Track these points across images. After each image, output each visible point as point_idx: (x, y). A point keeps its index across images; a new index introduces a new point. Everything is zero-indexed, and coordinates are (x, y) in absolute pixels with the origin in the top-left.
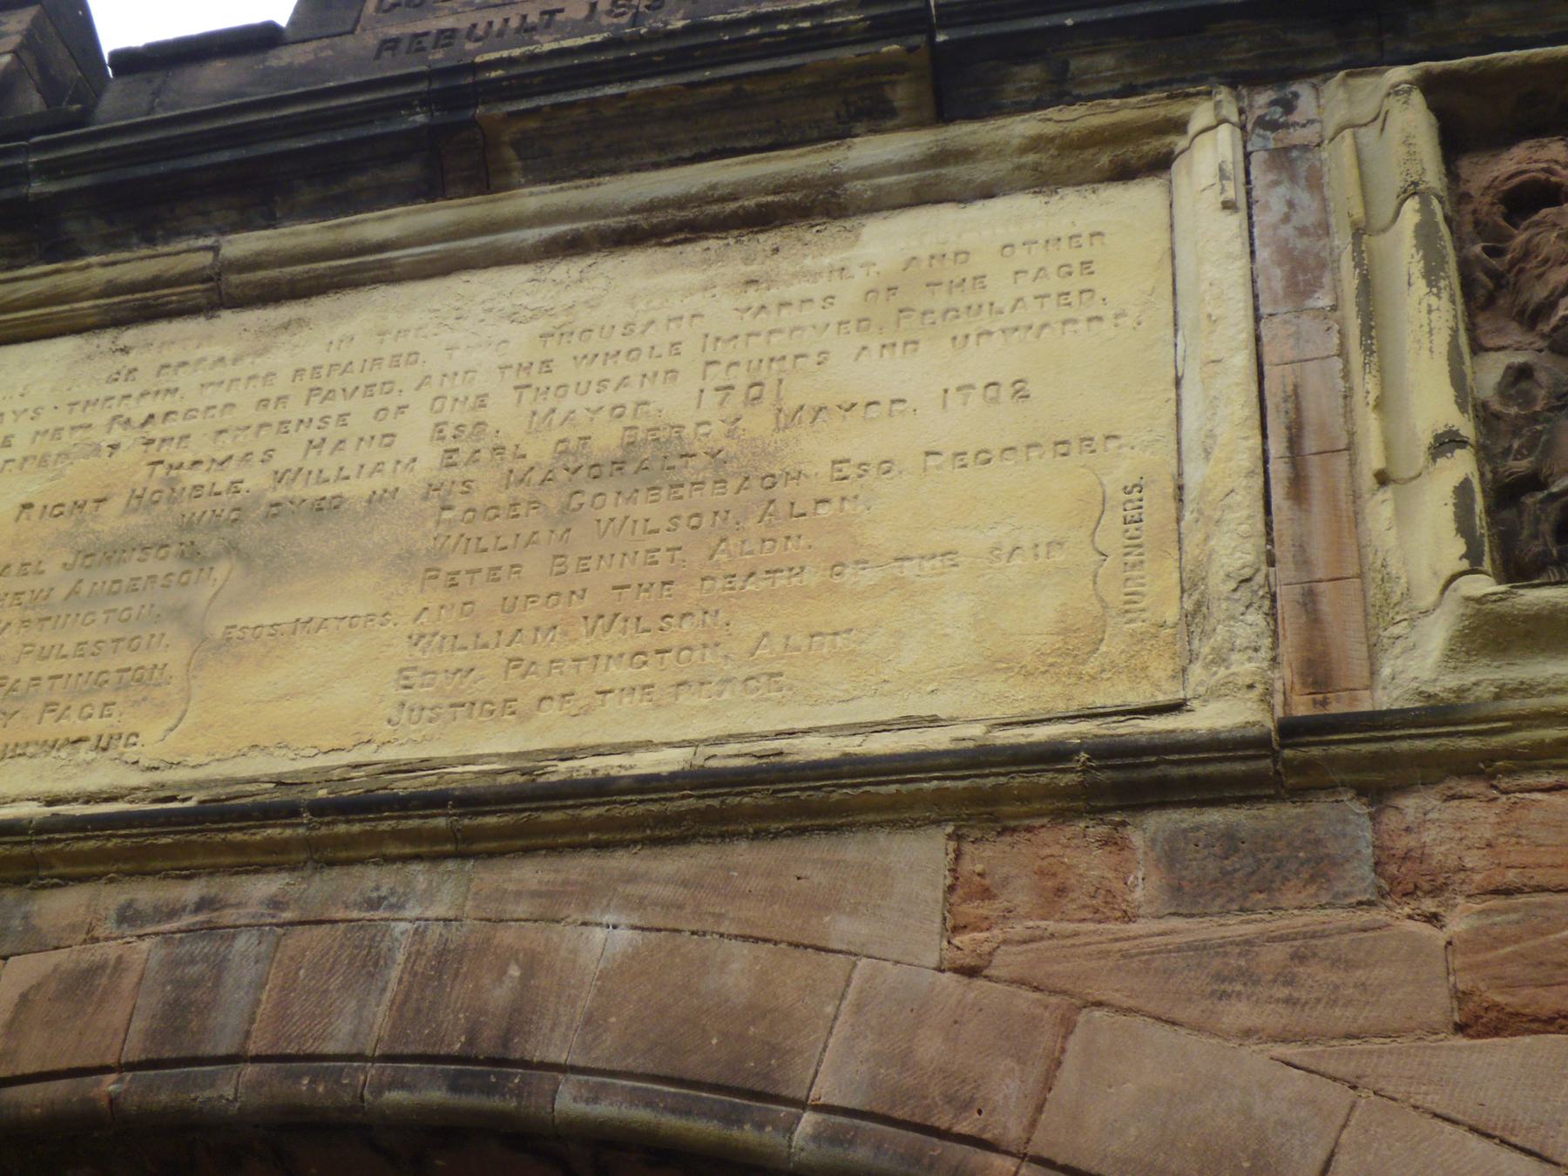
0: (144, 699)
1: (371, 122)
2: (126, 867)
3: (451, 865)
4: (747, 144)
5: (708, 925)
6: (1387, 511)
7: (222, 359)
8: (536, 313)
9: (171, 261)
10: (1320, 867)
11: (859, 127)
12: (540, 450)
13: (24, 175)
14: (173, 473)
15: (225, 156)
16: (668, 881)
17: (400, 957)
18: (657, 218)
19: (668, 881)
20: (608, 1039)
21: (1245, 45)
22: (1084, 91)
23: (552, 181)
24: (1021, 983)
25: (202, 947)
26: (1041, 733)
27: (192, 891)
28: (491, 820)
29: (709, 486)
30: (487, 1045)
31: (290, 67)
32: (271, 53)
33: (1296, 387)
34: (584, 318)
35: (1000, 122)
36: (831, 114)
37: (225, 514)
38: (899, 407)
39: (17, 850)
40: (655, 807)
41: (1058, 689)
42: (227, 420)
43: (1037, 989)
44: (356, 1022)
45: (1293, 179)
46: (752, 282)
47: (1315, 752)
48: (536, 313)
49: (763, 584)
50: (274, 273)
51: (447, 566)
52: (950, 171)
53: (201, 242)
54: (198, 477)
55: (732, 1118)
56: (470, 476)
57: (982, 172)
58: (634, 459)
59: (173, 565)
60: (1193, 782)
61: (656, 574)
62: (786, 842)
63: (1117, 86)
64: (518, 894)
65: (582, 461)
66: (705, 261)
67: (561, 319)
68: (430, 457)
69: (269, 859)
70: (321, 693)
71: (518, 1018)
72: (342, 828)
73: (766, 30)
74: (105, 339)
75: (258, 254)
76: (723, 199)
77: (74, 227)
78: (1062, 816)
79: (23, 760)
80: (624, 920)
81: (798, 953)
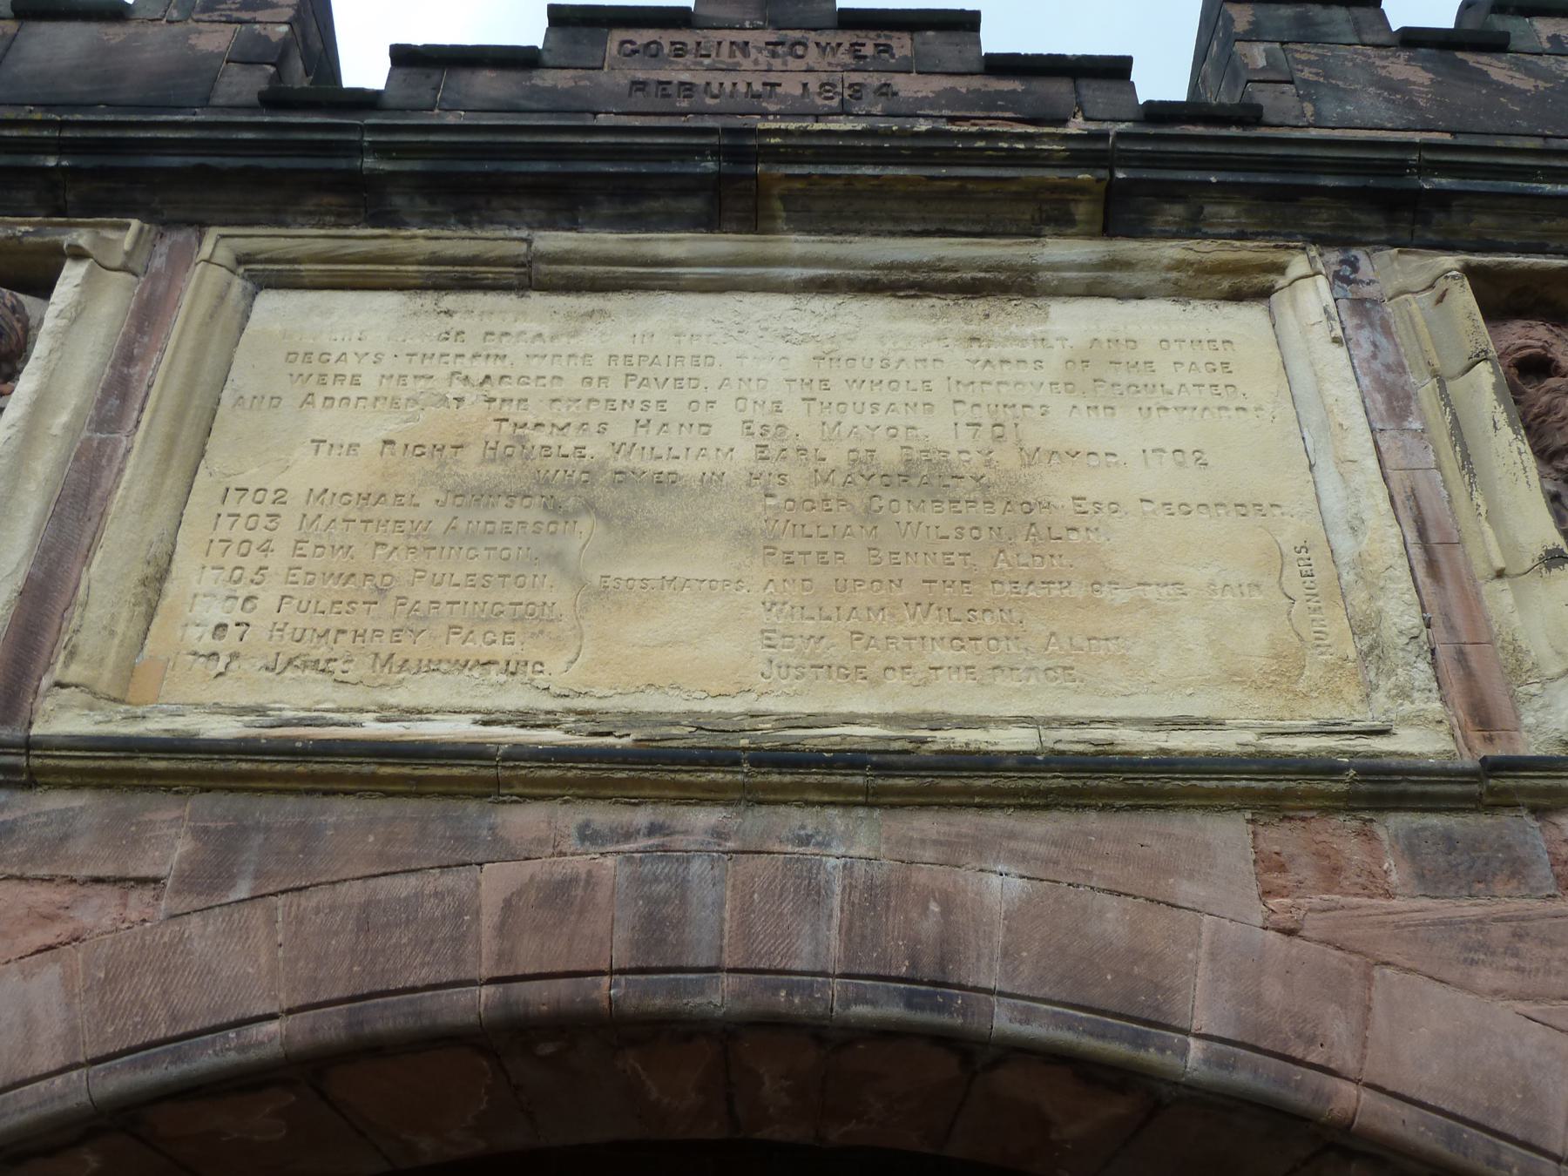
0: (541, 632)
1: (669, 161)
2: (581, 792)
3: (861, 812)
4: (961, 228)
5: (1081, 879)
6: (1507, 599)
7: (540, 335)
8: (806, 339)
9: (489, 244)
10: (1517, 869)
11: (1047, 230)
12: (836, 456)
13: (359, 150)
14: (519, 431)
15: (543, 167)
16: (1042, 840)
17: (838, 890)
18: (895, 276)
19: (1042, 840)
20: (1026, 970)
21: (1325, 216)
22: (1209, 230)
23: (809, 232)
24: (1328, 943)
25: (661, 868)
26: (1302, 744)
27: (642, 817)
28: (901, 782)
29: (980, 504)
30: (928, 970)
31: (554, 88)
32: (535, 73)
33: (1413, 490)
34: (847, 349)
35: (1154, 244)
36: (1028, 217)
37: (576, 475)
38: (1111, 459)
39: (484, 772)
40: (1032, 783)
41: (1282, 702)
42: (558, 390)
43: (1339, 948)
44: (815, 944)
45: (1372, 325)
46: (974, 339)
47: (1510, 782)
48: (806, 339)
49: (1042, 592)
50: (578, 269)
51: (783, 545)
52: (1116, 275)
53: (515, 233)
54: (540, 438)
55: (1140, 1042)
56: (783, 471)
57: (1137, 279)
58: (916, 475)
59: (534, 514)
60: (1423, 796)
61: (955, 573)
62: (1125, 815)
63: (1233, 231)
64: (923, 841)
65: (873, 470)
66: (933, 316)
67: (827, 347)
68: (745, 451)
69: (707, 796)
70: (700, 647)
71: (948, 948)
72: (775, 778)
73: (991, 145)
74: (428, 300)
75: (568, 252)
76: (945, 270)
77: (399, 201)
78: (1326, 811)
79: (437, 675)
80: (1013, 870)
81: (1155, 907)
